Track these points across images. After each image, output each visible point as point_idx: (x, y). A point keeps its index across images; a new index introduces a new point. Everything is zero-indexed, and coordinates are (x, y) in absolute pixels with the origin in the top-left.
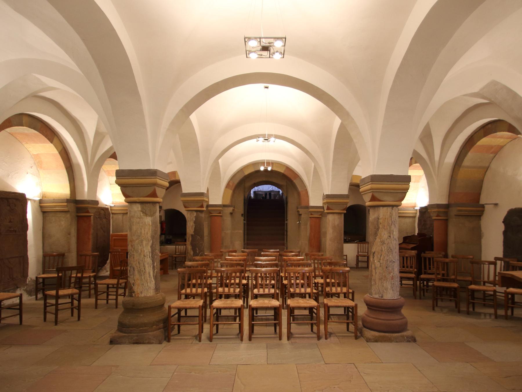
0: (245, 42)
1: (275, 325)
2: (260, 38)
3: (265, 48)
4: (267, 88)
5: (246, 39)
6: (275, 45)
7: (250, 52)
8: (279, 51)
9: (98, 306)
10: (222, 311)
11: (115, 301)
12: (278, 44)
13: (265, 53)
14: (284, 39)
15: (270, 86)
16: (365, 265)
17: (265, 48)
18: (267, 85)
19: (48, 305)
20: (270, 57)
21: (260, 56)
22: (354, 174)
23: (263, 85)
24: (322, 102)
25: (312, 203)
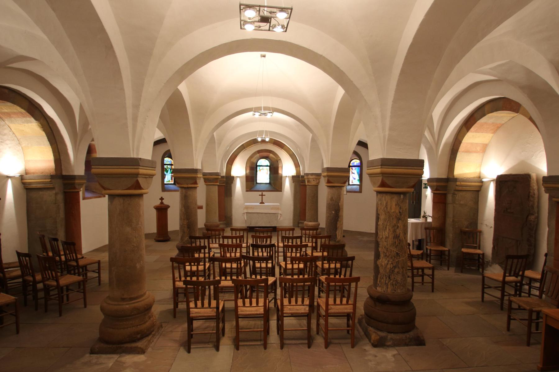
0: (240, 10)
1: (68, 290)
2: (260, 6)
3: (265, 20)
4: (264, 56)
5: (242, 7)
6: (277, 15)
7: (246, 22)
8: (281, 23)
9: (177, 315)
10: (88, 266)
11: (431, 284)
12: (282, 16)
13: (265, 26)
14: (290, 11)
15: (268, 54)
16: (420, 271)
17: (265, 20)
18: (263, 53)
19: (485, 286)
20: (269, 30)
21: (257, 28)
22: (371, 159)
23: (259, 54)
24: (331, 76)
25: (218, 263)
